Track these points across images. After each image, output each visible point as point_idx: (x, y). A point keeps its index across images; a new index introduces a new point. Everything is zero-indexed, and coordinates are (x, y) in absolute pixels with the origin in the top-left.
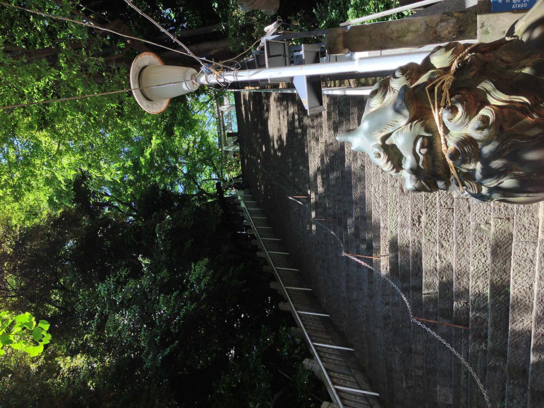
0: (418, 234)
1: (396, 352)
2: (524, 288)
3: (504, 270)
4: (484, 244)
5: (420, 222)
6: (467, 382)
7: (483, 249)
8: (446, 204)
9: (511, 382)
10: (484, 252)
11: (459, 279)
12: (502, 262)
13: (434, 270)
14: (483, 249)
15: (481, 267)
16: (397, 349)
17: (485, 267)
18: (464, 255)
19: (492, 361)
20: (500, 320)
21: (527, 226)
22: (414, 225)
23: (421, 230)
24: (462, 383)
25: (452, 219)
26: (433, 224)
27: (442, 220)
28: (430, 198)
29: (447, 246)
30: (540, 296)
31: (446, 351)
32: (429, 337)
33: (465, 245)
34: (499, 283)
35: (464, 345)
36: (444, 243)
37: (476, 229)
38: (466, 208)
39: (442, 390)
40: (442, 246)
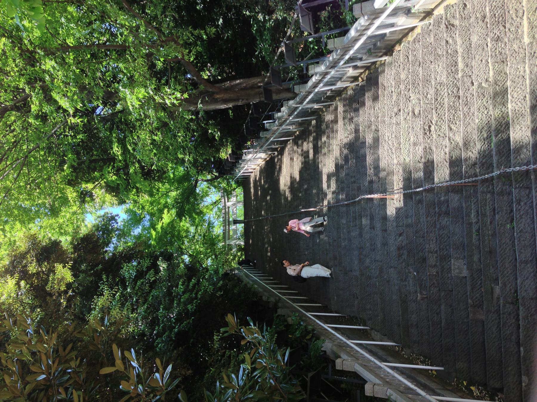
0: (429, 141)
1: (410, 273)
2: (520, 100)
3: (503, 104)
4: (485, 98)
5: (430, 131)
6: (479, 239)
7: (485, 103)
8: (453, 92)
9: (517, 186)
10: (486, 105)
11: (466, 145)
12: (501, 97)
13: (444, 161)
14: (485, 103)
15: (484, 119)
16: (411, 270)
17: (488, 118)
18: (469, 124)
19: (499, 186)
20: (503, 148)
21: (517, 50)
22: (426, 133)
23: (431, 138)
24: (474, 241)
25: (458, 104)
26: (442, 121)
27: (450, 107)
28: (439, 99)
29: (455, 128)
30: (532, 87)
31: (457, 224)
32: (442, 224)
33: (470, 114)
34: (500, 116)
35: (474, 204)
36: (452, 126)
37: (479, 88)
38: (469, 84)
39: (456, 263)
40: (451, 129)
